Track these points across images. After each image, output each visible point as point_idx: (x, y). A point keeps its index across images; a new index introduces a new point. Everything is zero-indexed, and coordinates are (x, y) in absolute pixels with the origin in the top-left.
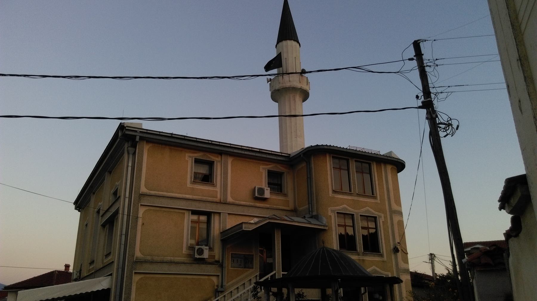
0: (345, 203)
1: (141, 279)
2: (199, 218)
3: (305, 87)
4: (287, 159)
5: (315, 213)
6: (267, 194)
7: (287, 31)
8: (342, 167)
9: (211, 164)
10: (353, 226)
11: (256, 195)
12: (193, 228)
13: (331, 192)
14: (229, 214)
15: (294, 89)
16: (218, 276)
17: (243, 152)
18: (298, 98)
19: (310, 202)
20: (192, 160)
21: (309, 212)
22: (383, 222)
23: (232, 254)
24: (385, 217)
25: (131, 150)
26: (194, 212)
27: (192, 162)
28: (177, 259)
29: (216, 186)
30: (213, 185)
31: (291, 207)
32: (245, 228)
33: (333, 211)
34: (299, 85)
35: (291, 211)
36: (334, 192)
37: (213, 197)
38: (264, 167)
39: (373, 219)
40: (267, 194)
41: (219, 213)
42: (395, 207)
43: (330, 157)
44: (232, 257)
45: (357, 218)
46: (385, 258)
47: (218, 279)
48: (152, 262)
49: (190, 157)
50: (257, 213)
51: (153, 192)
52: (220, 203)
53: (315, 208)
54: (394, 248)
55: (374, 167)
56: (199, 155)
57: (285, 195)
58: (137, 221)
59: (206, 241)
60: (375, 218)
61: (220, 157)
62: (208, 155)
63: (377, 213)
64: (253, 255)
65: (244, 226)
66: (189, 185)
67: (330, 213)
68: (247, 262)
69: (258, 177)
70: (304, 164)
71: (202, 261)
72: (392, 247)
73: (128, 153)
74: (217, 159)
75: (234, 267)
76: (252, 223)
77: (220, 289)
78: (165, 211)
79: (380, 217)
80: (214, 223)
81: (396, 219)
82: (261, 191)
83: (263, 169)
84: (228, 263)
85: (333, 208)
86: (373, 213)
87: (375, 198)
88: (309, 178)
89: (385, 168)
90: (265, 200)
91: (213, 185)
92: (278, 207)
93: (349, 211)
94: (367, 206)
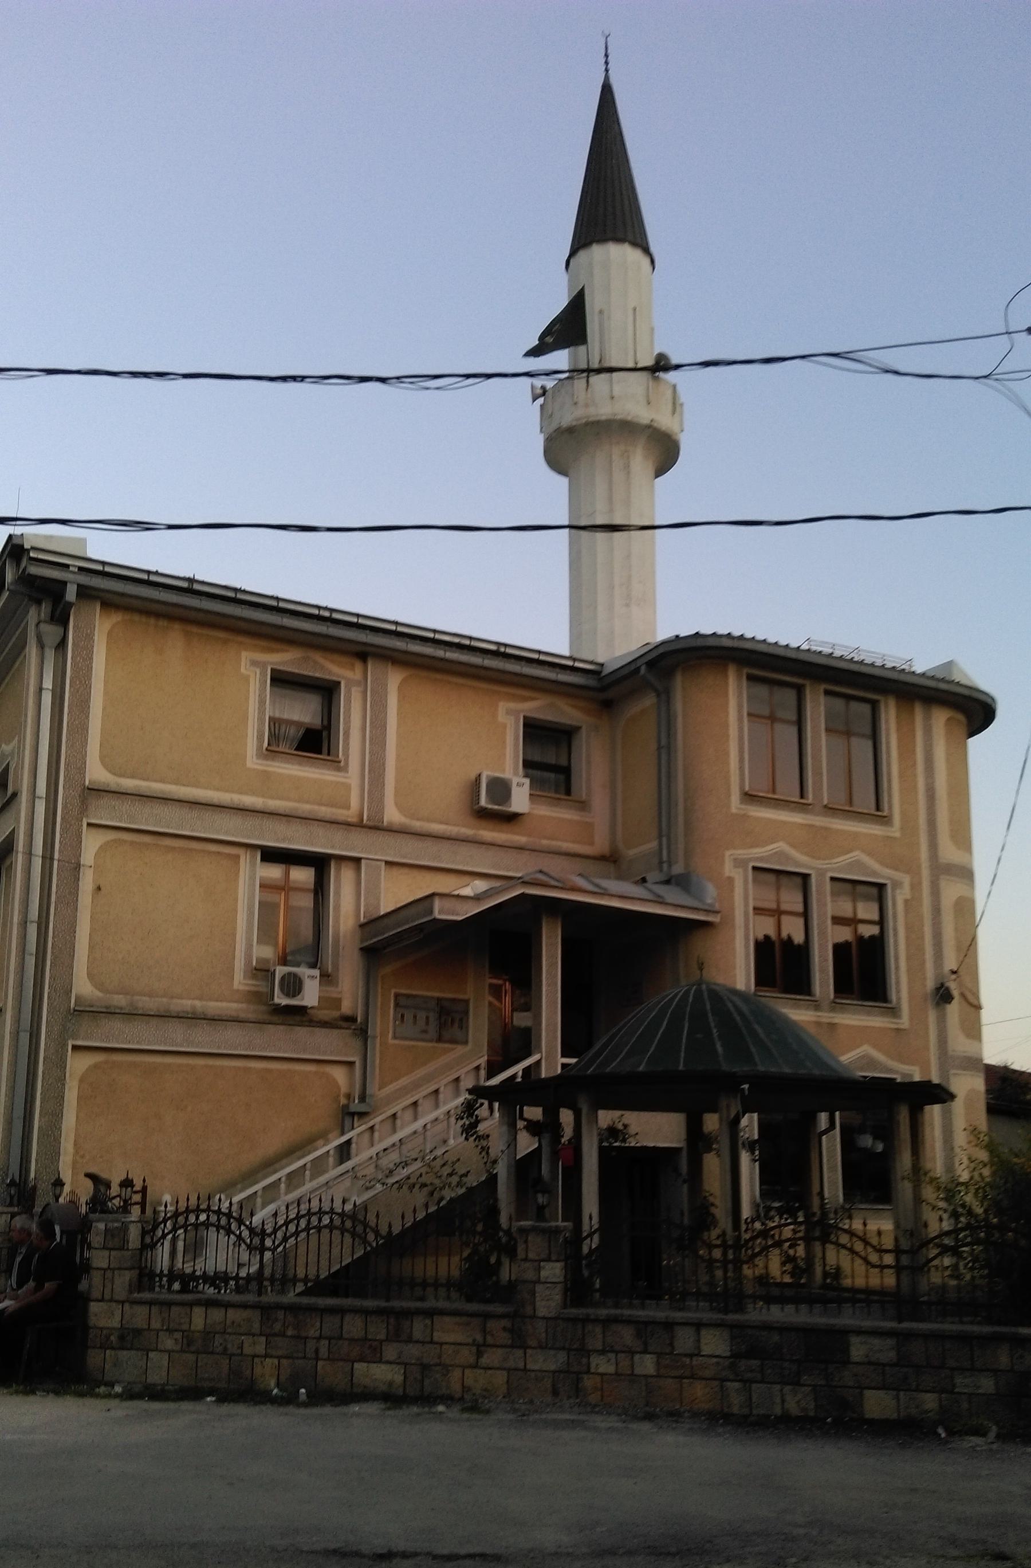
0: (782, 835)
1: (96, 1066)
2: (287, 874)
3: (665, 421)
4: (591, 682)
5: (678, 869)
6: (520, 800)
7: (608, 209)
8: (780, 714)
9: (327, 692)
10: (806, 915)
11: (483, 802)
12: (267, 909)
14: (388, 863)
15: (624, 429)
16: (351, 1064)
17: (440, 653)
18: (640, 462)
19: (664, 831)
20: (263, 674)
21: (661, 863)
22: (906, 901)
23: (397, 996)
24: (916, 886)
25: (52, 632)
26: (271, 855)
27: (263, 683)
28: (214, 1007)
29: (345, 769)
30: (337, 765)
31: (600, 844)
32: (441, 911)
33: (739, 863)
34: (643, 415)
35: (602, 858)
36: (749, 797)
38: (512, 705)
39: (874, 891)
40: (520, 800)
41: (357, 860)
43: (739, 677)
44: (397, 1005)
46: (905, 1021)
48: (131, 1015)
49: (254, 663)
51: (129, 784)
52: (360, 825)
53: (681, 853)
54: (938, 989)
55: (890, 714)
56: (286, 659)
57: (583, 806)
58: (77, 879)
59: (314, 952)
61: (359, 666)
62: (319, 661)
63: (887, 872)
64: (467, 1002)
65: (437, 903)
66: (253, 761)
67: (729, 869)
68: (448, 1021)
69: (491, 741)
70: (648, 701)
71: (296, 1015)
72: (930, 984)
73: (41, 646)
74: (349, 674)
76: (465, 896)
77: (356, 1106)
78: (174, 849)
80: (338, 893)
81: (951, 891)
82: (500, 789)
83: (509, 712)
84: (384, 1024)
85: (741, 853)
86: (875, 873)
88: (666, 748)
89: (927, 718)
90: (511, 818)
91: (337, 765)
92: (554, 843)
93: (797, 864)
94: (854, 848)
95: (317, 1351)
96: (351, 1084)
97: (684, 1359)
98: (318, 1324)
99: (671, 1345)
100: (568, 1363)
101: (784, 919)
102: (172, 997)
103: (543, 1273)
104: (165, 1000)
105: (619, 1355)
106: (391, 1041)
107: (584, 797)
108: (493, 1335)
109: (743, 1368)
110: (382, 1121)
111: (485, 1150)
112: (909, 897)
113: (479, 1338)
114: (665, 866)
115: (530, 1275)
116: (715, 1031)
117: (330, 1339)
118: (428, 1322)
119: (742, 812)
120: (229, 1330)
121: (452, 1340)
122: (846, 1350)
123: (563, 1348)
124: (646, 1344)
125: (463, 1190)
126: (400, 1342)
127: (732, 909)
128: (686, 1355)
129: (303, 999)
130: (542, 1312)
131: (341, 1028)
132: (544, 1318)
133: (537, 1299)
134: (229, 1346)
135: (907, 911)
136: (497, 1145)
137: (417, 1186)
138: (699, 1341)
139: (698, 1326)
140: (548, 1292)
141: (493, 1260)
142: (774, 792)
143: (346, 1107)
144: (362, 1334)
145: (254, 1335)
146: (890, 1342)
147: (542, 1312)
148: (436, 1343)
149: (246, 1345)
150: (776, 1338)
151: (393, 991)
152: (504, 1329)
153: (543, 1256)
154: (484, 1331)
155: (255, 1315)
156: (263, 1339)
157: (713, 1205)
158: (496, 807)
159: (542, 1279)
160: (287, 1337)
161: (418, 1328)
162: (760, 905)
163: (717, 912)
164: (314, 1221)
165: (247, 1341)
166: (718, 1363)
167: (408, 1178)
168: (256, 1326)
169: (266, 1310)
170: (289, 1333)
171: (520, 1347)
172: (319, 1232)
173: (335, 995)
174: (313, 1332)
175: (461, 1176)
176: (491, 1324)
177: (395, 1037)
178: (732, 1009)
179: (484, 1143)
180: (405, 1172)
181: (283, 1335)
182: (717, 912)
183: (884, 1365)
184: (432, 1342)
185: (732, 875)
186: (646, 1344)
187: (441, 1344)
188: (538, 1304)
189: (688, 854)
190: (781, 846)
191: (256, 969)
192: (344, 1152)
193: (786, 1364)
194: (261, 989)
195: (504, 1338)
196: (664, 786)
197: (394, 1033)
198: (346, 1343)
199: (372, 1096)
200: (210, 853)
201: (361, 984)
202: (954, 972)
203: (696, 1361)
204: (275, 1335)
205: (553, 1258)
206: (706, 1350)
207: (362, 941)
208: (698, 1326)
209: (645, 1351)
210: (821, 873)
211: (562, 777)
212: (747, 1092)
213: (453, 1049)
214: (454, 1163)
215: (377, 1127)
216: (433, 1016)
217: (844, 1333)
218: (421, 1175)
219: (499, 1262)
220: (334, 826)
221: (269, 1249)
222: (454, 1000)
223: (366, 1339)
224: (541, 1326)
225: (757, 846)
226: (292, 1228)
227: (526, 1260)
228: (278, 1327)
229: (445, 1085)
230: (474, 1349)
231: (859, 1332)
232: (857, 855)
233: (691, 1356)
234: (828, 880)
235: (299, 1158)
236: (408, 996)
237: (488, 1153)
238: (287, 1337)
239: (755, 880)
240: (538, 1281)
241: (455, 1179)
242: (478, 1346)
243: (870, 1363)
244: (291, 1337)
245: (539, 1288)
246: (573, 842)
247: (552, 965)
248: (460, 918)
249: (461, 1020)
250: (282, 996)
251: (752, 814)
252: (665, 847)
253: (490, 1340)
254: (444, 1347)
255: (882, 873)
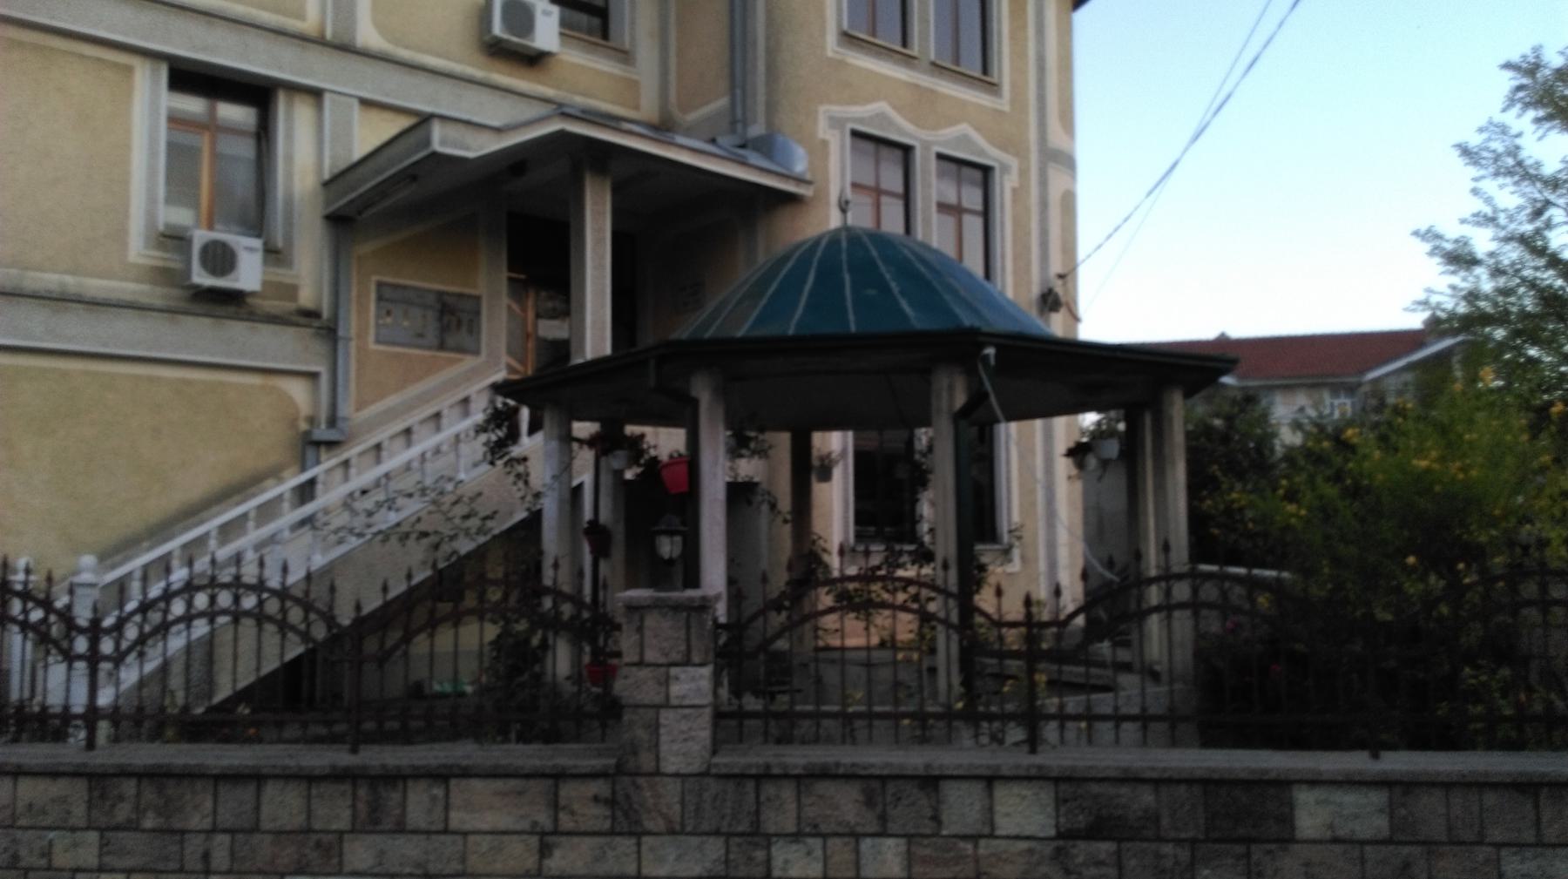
0: (884, 92)
5: (757, 130)
10: (907, 197)
11: (498, 29)
13: (831, 38)
14: (366, 103)
16: (313, 376)
19: (737, 78)
21: (733, 123)
22: (1014, 191)
23: (380, 285)
24: (1024, 173)
28: (95, 286)
32: (442, 140)
33: (836, 122)
36: (848, 38)
37: (285, 13)
39: (978, 175)
41: (316, 94)
42: (1056, 138)
44: (380, 298)
45: (925, 166)
47: (315, 390)
50: (495, 111)
52: (320, 41)
53: (761, 109)
57: (625, 56)
59: (256, 215)
60: (986, 171)
64: (478, 298)
67: (823, 131)
68: (452, 323)
71: (228, 302)
72: (1036, 291)
75: (394, 344)
77: (322, 433)
78: (21, 44)
79: (1005, 169)
80: (290, 136)
84: (362, 322)
85: (837, 110)
86: (982, 153)
87: (993, 88)
90: (534, 60)
93: (900, 130)
94: (952, 120)
95: (206, 856)
96: (316, 402)
97: (962, 844)
98: (209, 804)
99: (936, 818)
100: (727, 862)
101: (884, 199)
102: (27, 268)
103: (675, 689)
104: (13, 271)
105: (831, 842)
106: (372, 346)
107: (627, 46)
108: (573, 813)
109: (1080, 859)
110: (361, 454)
111: (524, 478)
112: (1016, 185)
113: (544, 819)
114: (739, 126)
115: (650, 694)
116: (893, 285)
117: (231, 832)
118: (438, 791)
119: (838, 57)
120: (23, 822)
121: (485, 827)
122: (1287, 819)
123: (717, 833)
124: (883, 818)
125: (488, 537)
126: (382, 832)
127: (827, 181)
128: (965, 837)
129: (237, 280)
130: (671, 764)
131: (297, 325)
132: (677, 775)
133: (664, 738)
134: (23, 852)
135: (1014, 201)
136: (541, 472)
137: (414, 536)
138: (991, 810)
139: (990, 780)
140: (684, 726)
141: (535, 641)
142: (874, 34)
143: (307, 433)
144: (298, 821)
145: (73, 829)
146: (1378, 798)
147: (671, 764)
148: (455, 833)
149: (58, 849)
150: (1147, 797)
151: (375, 278)
152: (596, 799)
153: (675, 657)
154: (555, 806)
155: (77, 792)
156: (93, 836)
157: (825, 550)
158: (515, 39)
159: (674, 702)
160: (144, 831)
161: (418, 803)
162: (859, 181)
163: (809, 183)
164: (224, 599)
165: (60, 839)
166: (1031, 851)
167: (398, 525)
168: (79, 812)
169: (98, 780)
170: (149, 823)
171: (631, 834)
172: (236, 620)
173: (288, 281)
174: (196, 821)
175: (485, 518)
176: (568, 791)
177: (378, 342)
178: (910, 255)
179: (520, 469)
180: (393, 518)
181: (132, 826)
182: (809, 183)
183: (1363, 843)
184: (446, 831)
185: (827, 137)
186: (883, 818)
187: (465, 834)
188: (664, 748)
189: (771, 108)
190: (882, 106)
191: (164, 236)
192: (306, 492)
193: (1167, 849)
194: (172, 265)
195: (595, 816)
196: (737, 17)
197: (377, 334)
198: (268, 838)
199: (345, 419)
200: (82, 56)
201: (326, 266)
202: (1061, 277)
203: (985, 848)
204: (117, 828)
205: (696, 659)
206: (1005, 826)
207: (328, 203)
208: (990, 780)
209: (883, 834)
210: (927, 145)
211: (596, 21)
212: (992, 361)
213: (460, 360)
214: (472, 499)
215: (354, 461)
216: (431, 315)
217: (1283, 784)
218: (419, 520)
219: (544, 645)
220: (281, 38)
221: (107, 658)
222: (460, 296)
223: (308, 830)
224: (672, 789)
225: (855, 103)
226: (178, 608)
227: (641, 664)
228: (123, 812)
229: (451, 407)
230: (534, 841)
231: (1314, 782)
232: (964, 128)
233: (974, 838)
234: (933, 157)
235: (238, 504)
236: (396, 287)
237: (526, 483)
238: (144, 831)
239: (853, 148)
240: (667, 705)
241: (474, 523)
242: (543, 834)
243: (1336, 840)
244: (154, 830)
245: (667, 717)
246: (613, 102)
247: (599, 242)
248: (471, 155)
249: (471, 321)
250: (203, 272)
251: (851, 60)
252: (739, 99)
253: (566, 822)
254: (471, 838)
255: (990, 154)
